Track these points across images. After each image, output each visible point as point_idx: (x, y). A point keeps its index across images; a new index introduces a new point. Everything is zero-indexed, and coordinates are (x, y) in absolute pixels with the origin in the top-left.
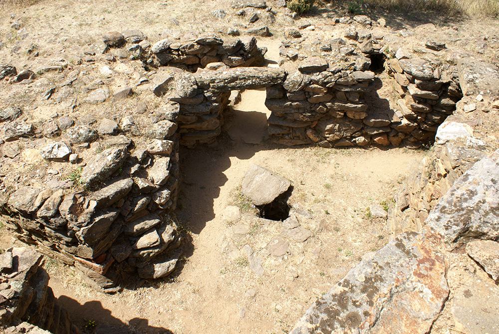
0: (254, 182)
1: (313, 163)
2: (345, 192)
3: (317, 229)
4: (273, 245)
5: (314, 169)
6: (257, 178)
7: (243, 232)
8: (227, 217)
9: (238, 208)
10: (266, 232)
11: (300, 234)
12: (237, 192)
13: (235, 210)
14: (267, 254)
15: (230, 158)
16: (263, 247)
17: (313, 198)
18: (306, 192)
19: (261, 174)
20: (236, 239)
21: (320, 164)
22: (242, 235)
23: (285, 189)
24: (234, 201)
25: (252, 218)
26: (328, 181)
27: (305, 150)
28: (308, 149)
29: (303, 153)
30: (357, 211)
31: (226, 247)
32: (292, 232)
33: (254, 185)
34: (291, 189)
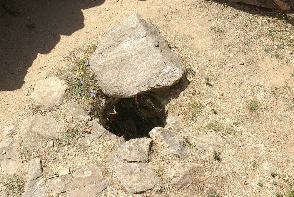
0: (118, 49)
1: (257, 49)
2: (279, 131)
3: (175, 180)
4: (79, 178)
5: (251, 62)
6: (126, 45)
7: (46, 133)
8: (37, 95)
9: (66, 87)
10: (86, 148)
11: (135, 178)
12: (82, 56)
13: (58, 86)
14: (59, 189)
15: (82, 10)
16: (61, 173)
17: (212, 118)
18: (205, 103)
19: (137, 38)
20: (27, 141)
21: (268, 58)
22: (43, 137)
23: (169, 82)
24: (69, 70)
25: (77, 113)
26: (261, 97)
27: (257, 19)
28: (262, 20)
29: (249, 24)
30: (277, 177)
31: (4, 148)
32: (124, 168)
33: (113, 55)
34: (181, 84)
